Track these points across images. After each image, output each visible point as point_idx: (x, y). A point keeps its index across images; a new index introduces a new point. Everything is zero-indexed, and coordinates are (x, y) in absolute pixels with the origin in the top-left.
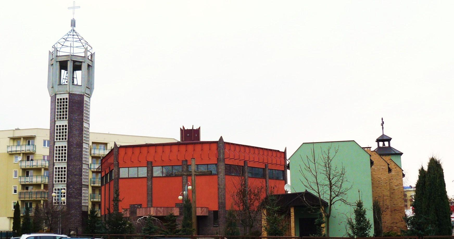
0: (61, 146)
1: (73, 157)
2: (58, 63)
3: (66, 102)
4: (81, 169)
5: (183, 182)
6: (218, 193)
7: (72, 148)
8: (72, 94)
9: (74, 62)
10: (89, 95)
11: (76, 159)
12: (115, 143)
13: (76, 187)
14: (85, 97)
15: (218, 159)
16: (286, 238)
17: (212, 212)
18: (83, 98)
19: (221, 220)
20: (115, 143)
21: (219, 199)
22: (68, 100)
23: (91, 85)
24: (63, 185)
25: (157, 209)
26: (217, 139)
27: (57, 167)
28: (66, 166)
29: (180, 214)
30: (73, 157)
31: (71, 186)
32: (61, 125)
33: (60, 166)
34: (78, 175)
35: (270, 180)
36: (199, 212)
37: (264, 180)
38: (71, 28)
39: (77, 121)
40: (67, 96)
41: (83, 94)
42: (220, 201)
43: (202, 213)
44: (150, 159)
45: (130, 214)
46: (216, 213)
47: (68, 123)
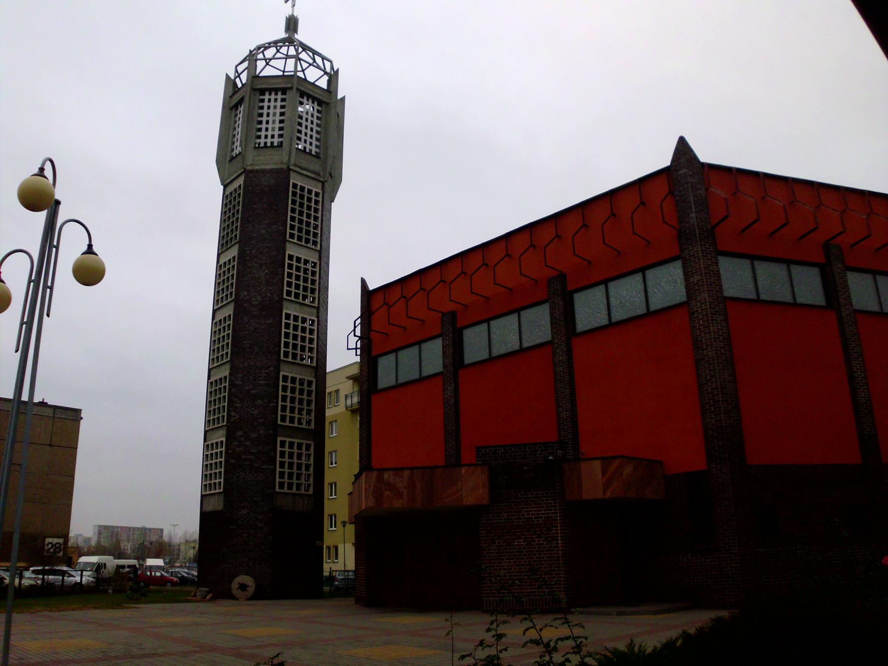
8: (251, 171)
13: (253, 435)
14: (292, 175)
41: (284, 167)
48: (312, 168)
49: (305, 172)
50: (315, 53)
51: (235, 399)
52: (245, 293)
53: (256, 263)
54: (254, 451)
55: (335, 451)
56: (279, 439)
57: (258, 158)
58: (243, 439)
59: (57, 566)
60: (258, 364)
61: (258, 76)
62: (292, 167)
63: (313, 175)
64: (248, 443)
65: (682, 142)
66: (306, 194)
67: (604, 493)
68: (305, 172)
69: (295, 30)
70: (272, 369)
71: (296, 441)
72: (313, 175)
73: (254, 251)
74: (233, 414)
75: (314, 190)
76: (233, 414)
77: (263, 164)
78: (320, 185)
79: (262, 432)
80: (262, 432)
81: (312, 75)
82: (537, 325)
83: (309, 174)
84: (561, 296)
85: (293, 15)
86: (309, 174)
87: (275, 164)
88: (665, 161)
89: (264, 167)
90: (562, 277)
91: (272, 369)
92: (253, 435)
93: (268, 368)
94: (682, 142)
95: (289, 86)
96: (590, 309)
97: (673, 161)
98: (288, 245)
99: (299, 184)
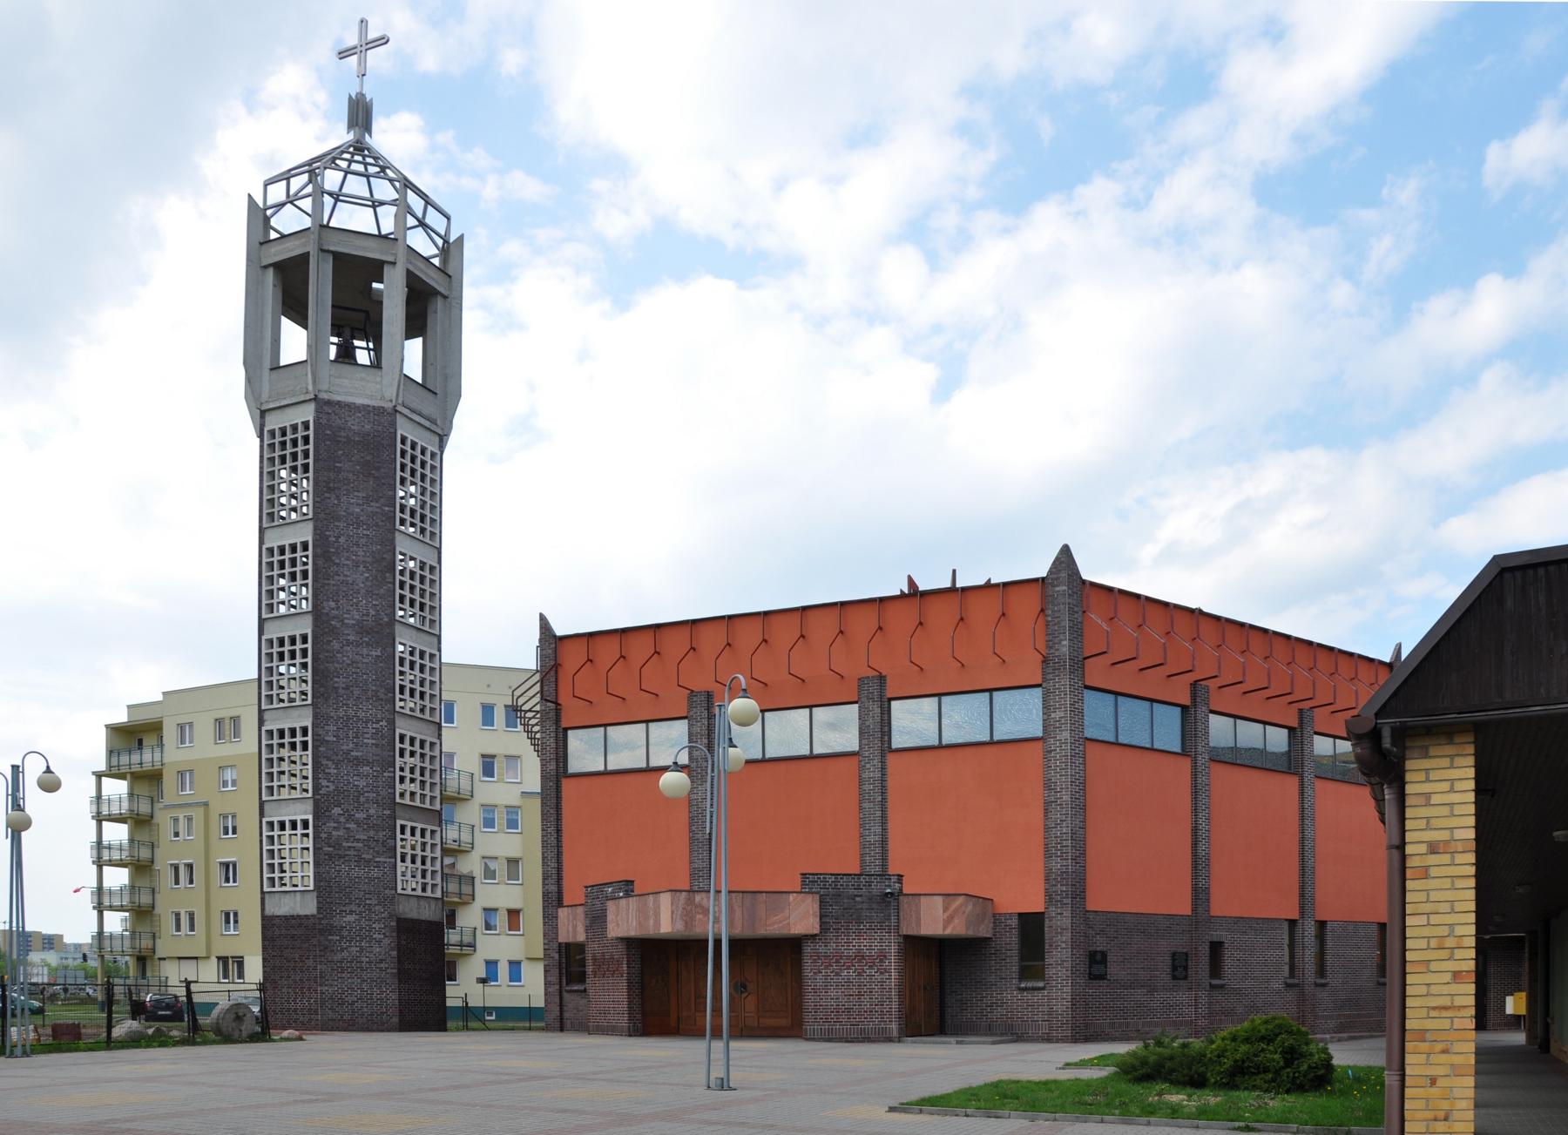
0: (286, 634)
1: (340, 682)
2: (271, 271)
3: (306, 440)
4: (388, 739)
5: (861, 782)
6: (1047, 829)
7: (336, 645)
8: (329, 403)
9: (338, 257)
10: (434, 422)
11: (357, 692)
12: (542, 618)
13: (360, 816)
14: (400, 420)
15: (1045, 661)
16: (314, 564)
17: (1014, 922)
18: (393, 424)
19: (1060, 956)
20: (542, 618)
21: (1048, 855)
22: (311, 432)
23: (446, 378)
24: (299, 806)
25: (690, 901)
26: (1039, 568)
27: (275, 727)
28: (308, 723)
29: (824, 927)
30: (340, 682)
31: (337, 811)
32: (287, 542)
33: (286, 726)
34: (368, 763)
35: (1319, 784)
36: (933, 920)
37: (1295, 780)
38: (341, 135)
39: (358, 524)
40: (307, 413)
41: (388, 406)
42: (1057, 865)
43: (947, 922)
44: (702, 683)
45: (586, 931)
46: (1031, 925)
47: (315, 534)
48: (425, 412)
49: (417, 418)
50: (407, 184)
51: (324, 762)
52: (332, 604)
53: (348, 559)
54: (362, 837)
55: (191, 771)
56: (399, 822)
57: (338, 381)
58: (342, 819)
59: (1133, 1054)
60: (361, 714)
61: (327, 226)
62: (399, 408)
63: (427, 424)
64: (352, 826)
65: (1066, 551)
66: (418, 452)
67: (945, 928)
68: (417, 418)
69: (367, 127)
70: (384, 723)
71: (420, 826)
72: (427, 424)
73: (342, 540)
74: (324, 783)
75: (430, 448)
76: (324, 783)
77: (346, 394)
78: (437, 439)
79: (372, 811)
80: (372, 811)
81: (419, 242)
82: (837, 729)
83: (423, 421)
84: (876, 700)
85: (361, 95)
86: (423, 421)
87: (371, 397)
88: (1040, 569)
89: (350, 399)
90: (882, 678)
91: (384, 723)
92: (360, 816)
93: (378, 722)
94: (1066, 551)
95: (390, 259)
96: (913, 721)
97: (1050, 572)
98: (399, 538)
99: (410, 437)
